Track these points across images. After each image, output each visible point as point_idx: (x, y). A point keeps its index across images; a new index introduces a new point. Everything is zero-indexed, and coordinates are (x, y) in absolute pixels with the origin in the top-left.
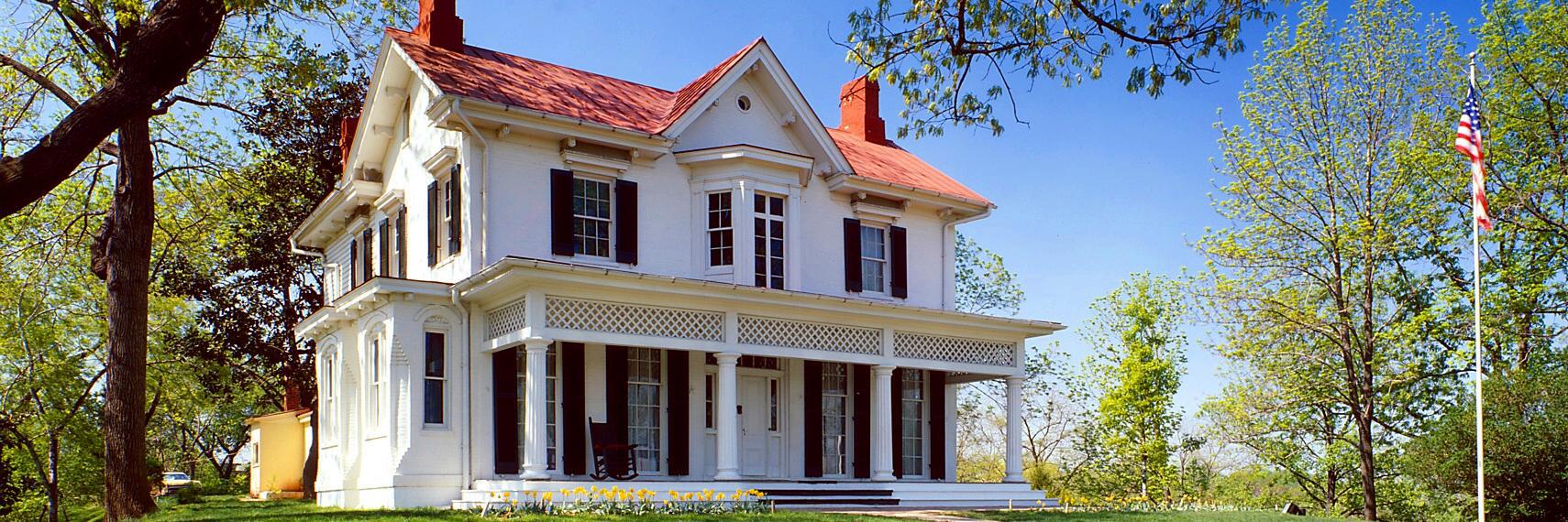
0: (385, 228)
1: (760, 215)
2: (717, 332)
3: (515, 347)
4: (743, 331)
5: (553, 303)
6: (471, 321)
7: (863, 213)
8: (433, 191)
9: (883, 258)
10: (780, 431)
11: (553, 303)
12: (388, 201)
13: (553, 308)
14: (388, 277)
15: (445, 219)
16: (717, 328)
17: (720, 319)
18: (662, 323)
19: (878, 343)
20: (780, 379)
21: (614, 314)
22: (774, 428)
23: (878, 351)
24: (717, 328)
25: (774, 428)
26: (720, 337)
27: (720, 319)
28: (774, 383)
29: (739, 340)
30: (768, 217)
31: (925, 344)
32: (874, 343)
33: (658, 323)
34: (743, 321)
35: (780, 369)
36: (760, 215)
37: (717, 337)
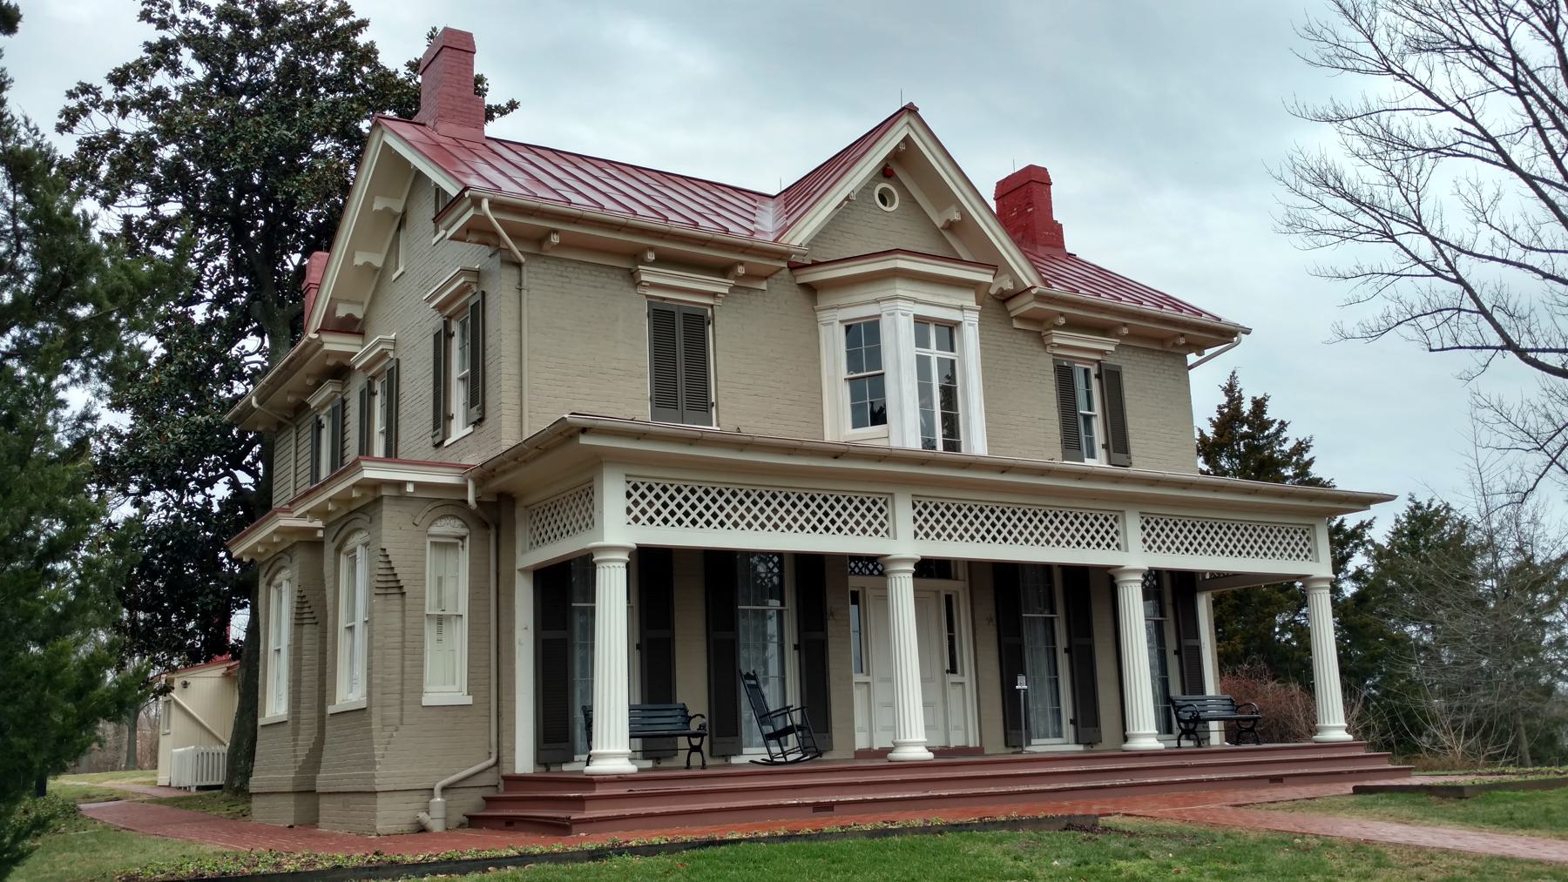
0: (368, 395)
1: (923, 352)
2: (1113, 539)
3: (570, 561)
4: (920, 520)
5: (636, 488)
6: (977, 638)
7: (1061, 346)
8: (442, 340)
9: (1090, 410)
10: (963, 675)
11: (636, 488)
12: (371, 355)
13: (636, 495)
14: (319, 285)
15: (457, 369)
16: (881, 517)
17: (885, 503)
18: (693, 507)
19: (1116, 533)
20: (957, 593)
21: (820, 507)
22: (953, 670)
23: (1118, 546)
24: (881, 517)
25: (953, 670)
26: (887, 532)
27: (885, 503)
28: (949, 599)
29: (916, 534)
30: (934, 353)
31: (1097, 525)
32: (1112, 533)
33: (686, 506)
34: (919, 507)
35: (957, 579)
36: (923, 352)
37: (882, 531)
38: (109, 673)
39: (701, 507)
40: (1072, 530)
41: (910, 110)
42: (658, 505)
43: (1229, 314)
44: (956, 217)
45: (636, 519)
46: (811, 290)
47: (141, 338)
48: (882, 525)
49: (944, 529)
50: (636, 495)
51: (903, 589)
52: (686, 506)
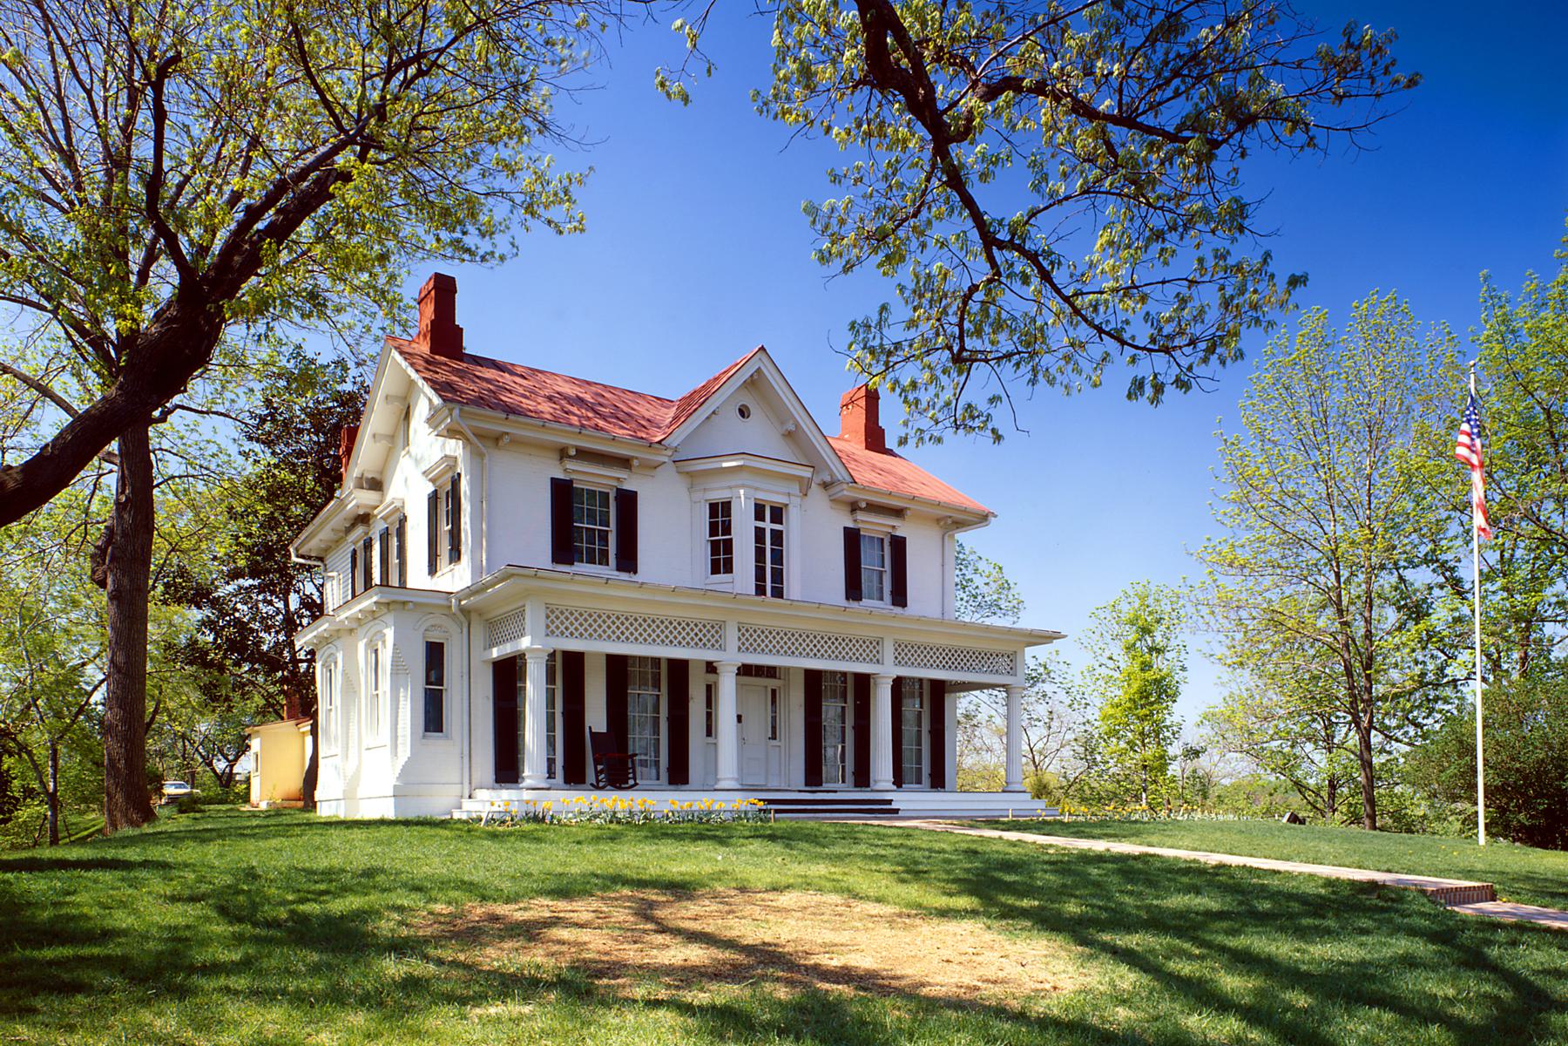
0: (385, 537)
1: (760, 524)
4: (743, 639)
11: (552, 612)
13: (553, 617)
18: (609, 627)
22: (774, 737)
25: (774, 737)
28: (774, 692)
29: (739, 648)
30: (768, 525)
32: (717, 637)
36: (760, 524)
38: (108, 325)
39: (632, 629)
40: (804, 645)
41: (762, 349)
42: (692, 634)
43: (986, 506)
44: (792, 428)
45: (553, 632)
46: (691, 475)
47: (255, 227)
48: (717, 641)
49: (595, 631)
50: (553, 617)
51: (728, 685)
52: (595, 626)
